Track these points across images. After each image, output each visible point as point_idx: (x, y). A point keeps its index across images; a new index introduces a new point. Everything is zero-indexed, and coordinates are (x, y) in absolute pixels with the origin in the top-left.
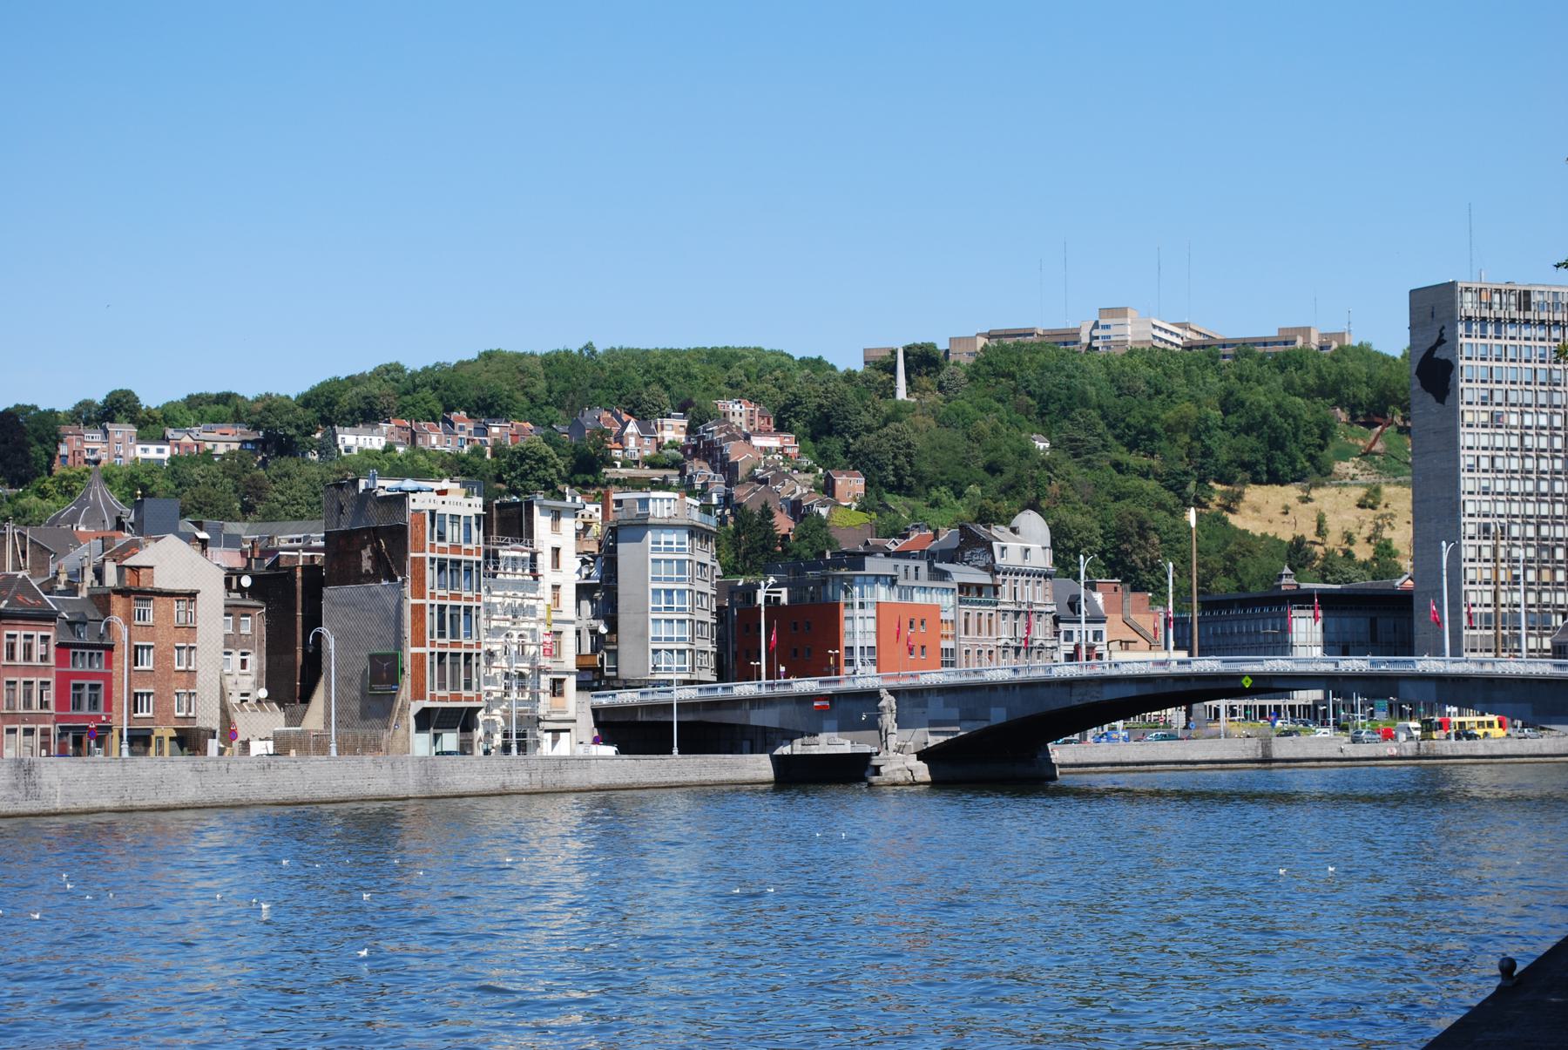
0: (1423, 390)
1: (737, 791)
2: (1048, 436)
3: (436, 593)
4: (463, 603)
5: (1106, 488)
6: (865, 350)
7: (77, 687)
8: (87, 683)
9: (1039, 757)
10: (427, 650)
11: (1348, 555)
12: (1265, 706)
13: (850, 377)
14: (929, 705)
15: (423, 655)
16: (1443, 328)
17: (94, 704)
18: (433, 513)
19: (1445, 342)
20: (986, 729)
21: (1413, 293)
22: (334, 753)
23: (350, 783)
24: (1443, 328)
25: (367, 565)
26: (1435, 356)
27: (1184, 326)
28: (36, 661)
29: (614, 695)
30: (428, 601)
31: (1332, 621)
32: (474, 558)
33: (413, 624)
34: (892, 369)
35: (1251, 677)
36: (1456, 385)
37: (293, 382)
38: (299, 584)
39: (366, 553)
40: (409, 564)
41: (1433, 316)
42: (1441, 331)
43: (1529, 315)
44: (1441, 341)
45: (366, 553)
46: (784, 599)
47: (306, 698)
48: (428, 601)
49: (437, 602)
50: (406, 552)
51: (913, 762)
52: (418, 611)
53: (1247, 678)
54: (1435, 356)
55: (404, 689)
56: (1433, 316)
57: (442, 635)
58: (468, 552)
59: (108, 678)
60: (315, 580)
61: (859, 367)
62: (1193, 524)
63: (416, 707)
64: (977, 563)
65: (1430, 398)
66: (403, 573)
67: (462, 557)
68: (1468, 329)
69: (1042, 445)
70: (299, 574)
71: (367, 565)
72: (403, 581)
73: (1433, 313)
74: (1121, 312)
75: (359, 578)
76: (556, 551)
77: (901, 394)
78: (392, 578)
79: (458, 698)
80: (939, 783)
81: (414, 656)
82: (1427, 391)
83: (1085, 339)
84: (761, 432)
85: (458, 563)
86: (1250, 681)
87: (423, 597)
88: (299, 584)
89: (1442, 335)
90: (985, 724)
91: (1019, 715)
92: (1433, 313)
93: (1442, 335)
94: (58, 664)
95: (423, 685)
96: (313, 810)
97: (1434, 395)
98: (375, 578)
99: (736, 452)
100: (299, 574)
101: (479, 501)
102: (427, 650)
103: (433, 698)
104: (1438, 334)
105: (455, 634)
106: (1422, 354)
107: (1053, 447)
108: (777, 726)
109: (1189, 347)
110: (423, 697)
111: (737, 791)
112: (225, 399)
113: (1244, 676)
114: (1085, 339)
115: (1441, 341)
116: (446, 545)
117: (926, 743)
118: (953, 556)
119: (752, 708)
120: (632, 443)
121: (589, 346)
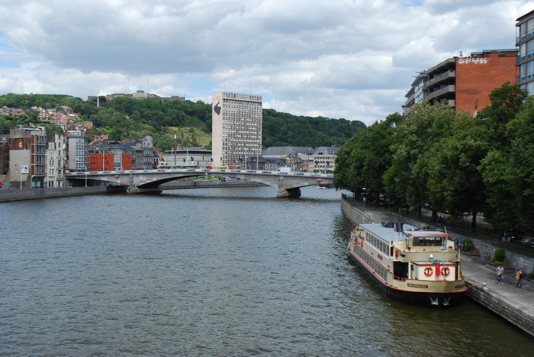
2: (129, 116)
4: (42, 154)
10: (35, 164)
11: (188, 141)
18: (36, 135)
23: (26, 194)
25: (21, 146)
30: (35, 154)
34: (96, 101)
39: (21, 143)
45: (21, 143)
48: (35, 154)
51: (137, 189)
55: (505, 301)
58: (43, 144)
69: (128, 117)
71: (21, 146)
75: (19, 149)
76: (60, 143)
77: (98, 106)
79: (41, 174)
84: (71, 113)
85: (41, 146)
90: (152, 181)
95: (34, 172)
98: (23, 149)
102: (35, 164)
103: (36, 174)
105: (40, 161)
110: (34, 174)
116: (39, 142)
121: (32, 93)
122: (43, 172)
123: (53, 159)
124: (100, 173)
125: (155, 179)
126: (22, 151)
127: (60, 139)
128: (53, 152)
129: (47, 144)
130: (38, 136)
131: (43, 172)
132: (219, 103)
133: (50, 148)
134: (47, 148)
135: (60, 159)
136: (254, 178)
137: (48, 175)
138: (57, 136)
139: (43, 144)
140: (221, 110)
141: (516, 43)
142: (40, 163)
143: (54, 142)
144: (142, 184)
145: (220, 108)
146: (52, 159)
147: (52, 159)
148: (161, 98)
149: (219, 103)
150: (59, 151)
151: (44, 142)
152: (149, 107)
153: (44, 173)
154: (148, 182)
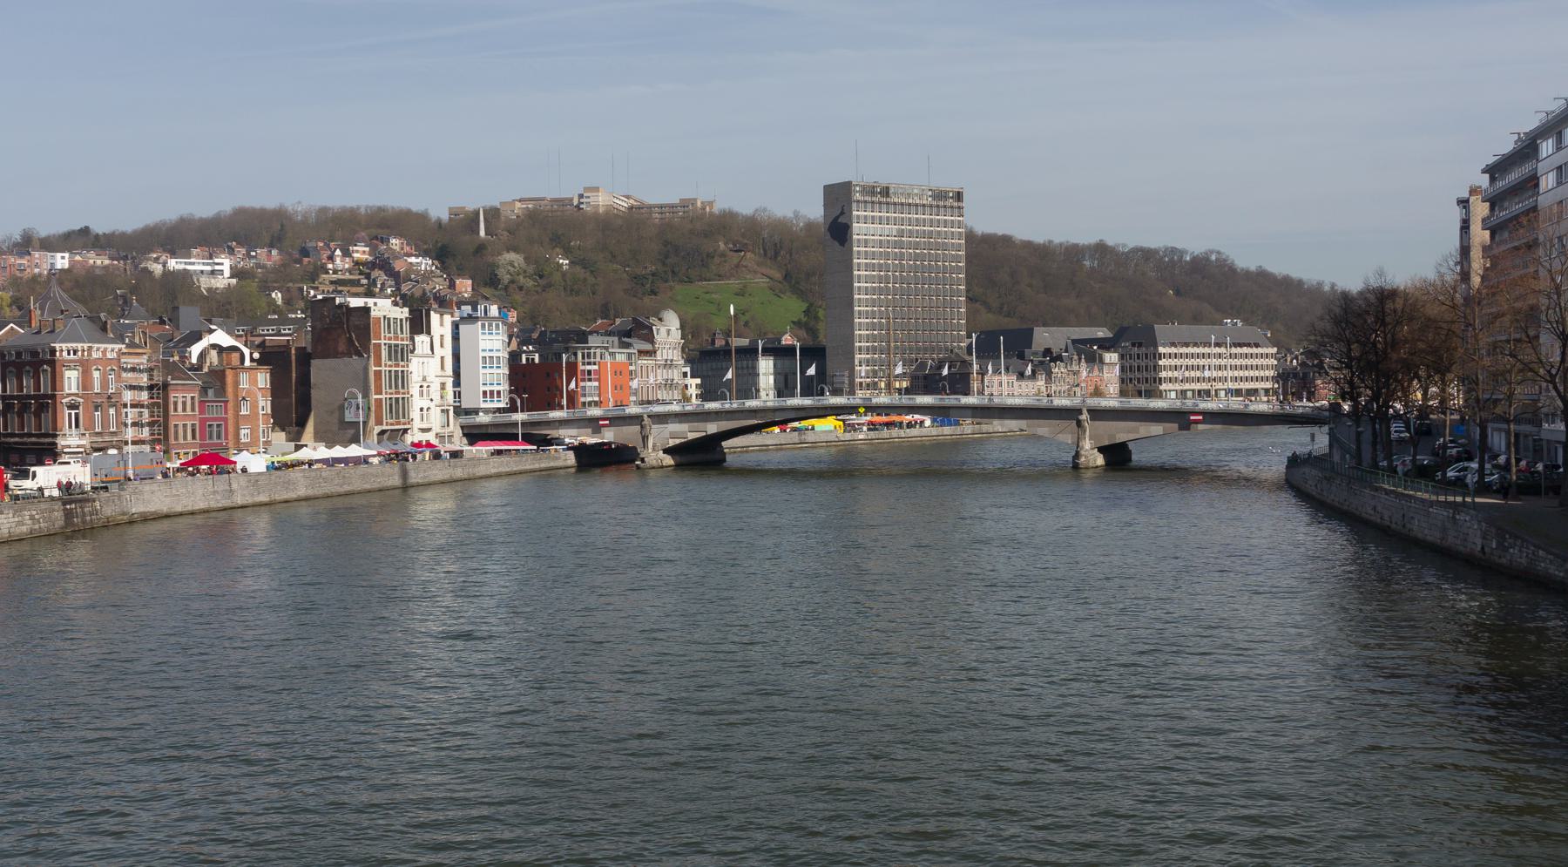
1: (549, 475)
3: (386, 366)
4: (400, 369)
5: (1516, 369)
6: (450, 208)
7: (210, 426)
8: (215, 423)
10: (383, 396)
13: (439, 223)
15: (381, 399)
17: (219, 437)
18: (385, 317)
21: (825, 187)
27: (628, 197)
28: (189, 411)
30: (383, 368)
31: (779, 362)
32: (405, 343)
33: (375, 381)
36: (851, 237)
37: (129, 222)
38: (293, 357)
40: (372, 347)
43: (889, 200)
44: (842, 213)
46: (537, 361)
47: (302, 424)
49: (388, 369)
50: (370, 340)
52: (377, 374)
57: (390, 388)
59: (226, 420)
60: (305, 358)
61: (445, 217)
62: (732, 313)
63: (377, 429)
65: (837, 243)
66: (368, 352)
67: (400, 342)
68: (858, 207)
70: (293, 352)
72: (369, 357)
74: (596, 189)
75: (336, 354)
78: (360, 355)
80: (1106, 470)
81: (376, 400)
83: (576, 203)
87: (380, 366)
88: (293, 357)
94: (201, 413)
96: (347, 501)
99: (399, 266)
100: (293, 352)
101: (406, 310)
102: (383, 396)
107: (571, 263)
109: (631, 208)
110: (382, 424)
111: (549, 475)
112: (85, 231)
114: (576, 203)
115: (842, 213)
118: (628, 334)
120: (338, 261)
122: (404, 417)
123: (428, 379)
124: (555, 414)
125: (712, 428)
126: (346, 359)
127: (442, 325)
128: (425, 360)
129: (412, 339)
130: (389, 319)
131: (404, 417)
133: (418, 351)
134: (412, 352)
135: (443, 380)
137: (417, 424)
138: (435, 317)
139: (402, 340)
141: (496, 204)
142: (396, 393)
143: (429, 333)
144: (678, 441)
146: (424, 379)
147: (424, 379)
148: (650, 207)
150: (442, 358)
151: (404, 335)
152: (558, 241)
153: (406, 420)
154: (692, 436)
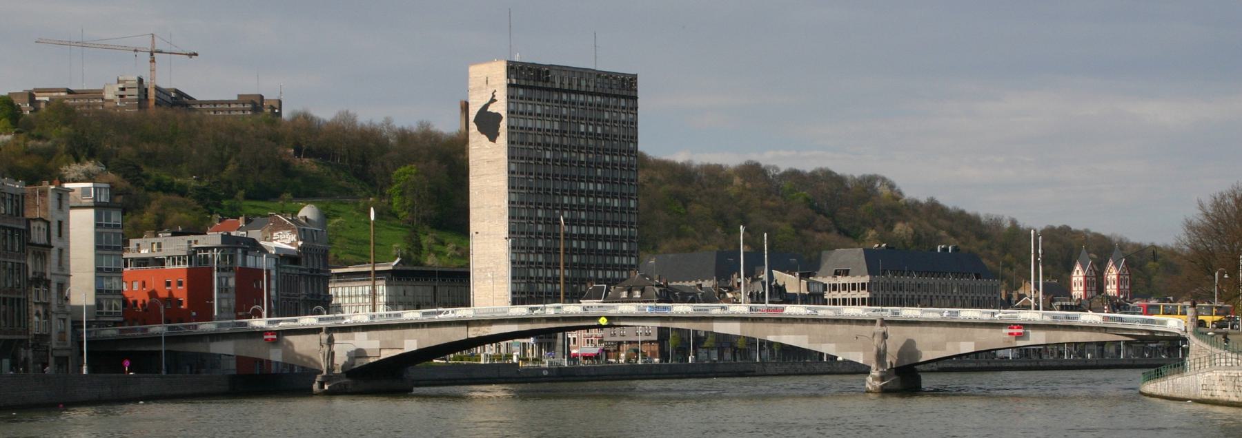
0: (479, 133)
9: (405, 375)
12: (525, 343)
14: (356, 338)
16: (495, 91)
19: (496, 101)
20: (400, 355)
22: (164, 373)
24: (495, 91)
26: (489, 110)
29: (993, 314)
31: (392, 288)
35: (606, 317)
41: (487, 83)
42: (493, 94)
53: (603, 318)
54: (489, 110)
56: (487, 83)
64: (283, 241)
65: (485, 138)
73: (487, 81)
82: (482, 133)
86: (606, 320)
89: (494, 96)
90: (400, 352)
91: (426, 345)
92: (487, 81)
93: (494, 96)
97: (487, 136)
104: (491, 96)
106: (479, 108)
108: (973, 351)
113: (600, 317)
117: (353, 365)
119: (212, 340)
132: (493, 100)
136: (776, 334)
140: (503, 125)
145: (498, 117)
149: (493, 100)
